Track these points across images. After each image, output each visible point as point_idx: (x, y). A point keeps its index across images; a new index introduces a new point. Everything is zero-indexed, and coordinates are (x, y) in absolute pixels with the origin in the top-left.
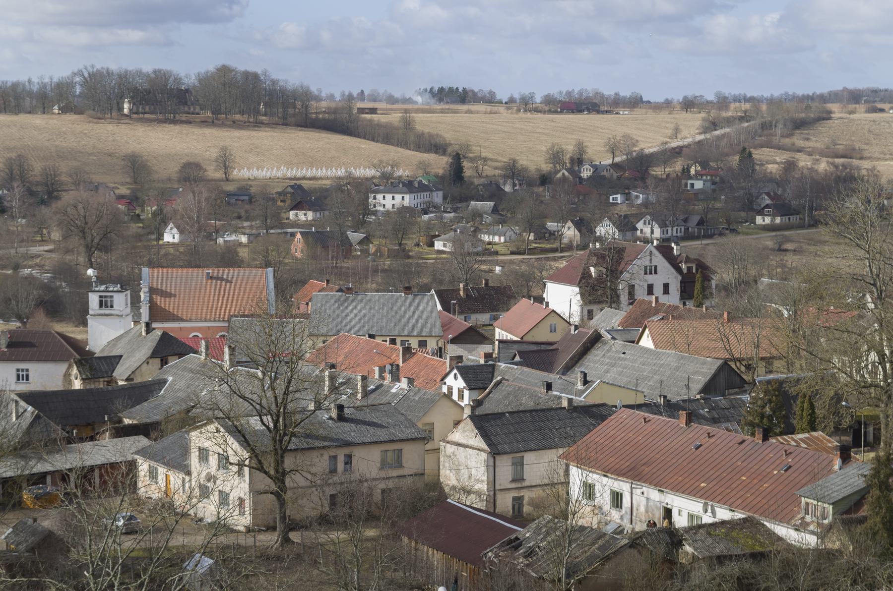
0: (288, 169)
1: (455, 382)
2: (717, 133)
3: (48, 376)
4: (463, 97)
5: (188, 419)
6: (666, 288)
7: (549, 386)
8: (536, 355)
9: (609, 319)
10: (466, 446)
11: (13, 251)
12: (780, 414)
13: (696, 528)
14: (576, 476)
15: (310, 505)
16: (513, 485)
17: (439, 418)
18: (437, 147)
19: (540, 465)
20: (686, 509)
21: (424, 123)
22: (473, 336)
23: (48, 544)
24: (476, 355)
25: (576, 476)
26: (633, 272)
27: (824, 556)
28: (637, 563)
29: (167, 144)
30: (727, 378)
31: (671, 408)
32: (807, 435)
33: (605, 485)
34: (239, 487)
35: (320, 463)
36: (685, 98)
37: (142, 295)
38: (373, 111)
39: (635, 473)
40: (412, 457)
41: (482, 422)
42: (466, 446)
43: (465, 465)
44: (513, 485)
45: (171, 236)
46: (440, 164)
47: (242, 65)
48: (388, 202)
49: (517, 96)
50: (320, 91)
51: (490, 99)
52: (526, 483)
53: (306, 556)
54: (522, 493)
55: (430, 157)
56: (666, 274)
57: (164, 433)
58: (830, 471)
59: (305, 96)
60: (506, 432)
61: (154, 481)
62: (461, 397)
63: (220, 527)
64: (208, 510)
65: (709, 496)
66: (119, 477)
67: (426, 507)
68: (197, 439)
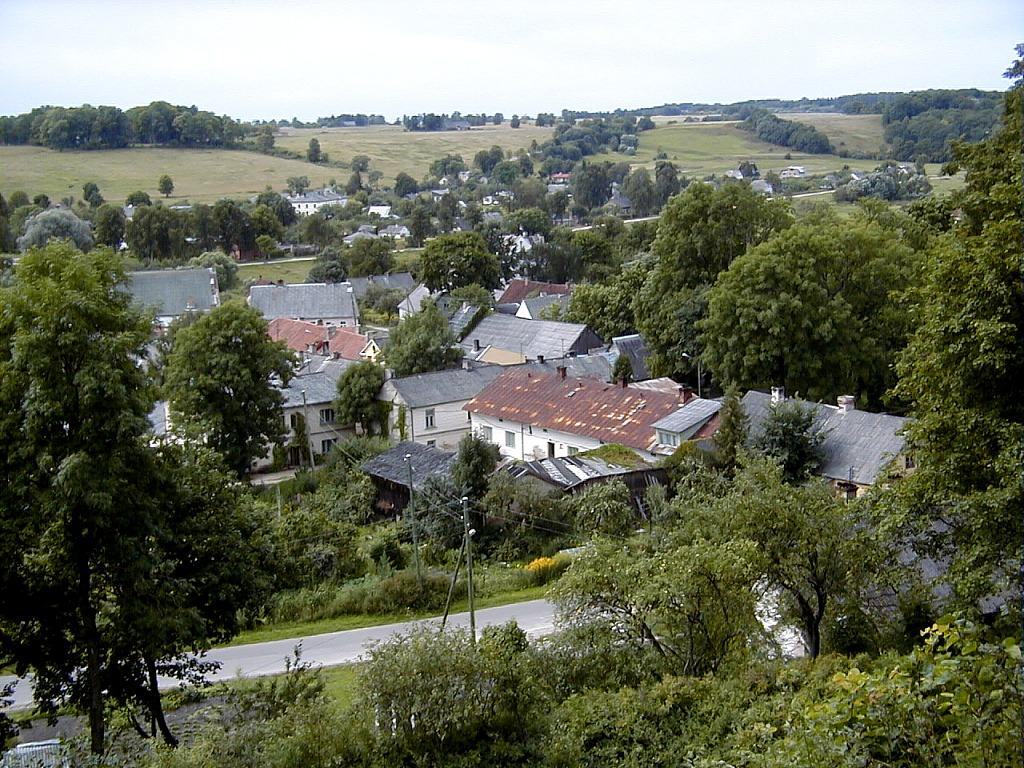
29: (124, 176)
51: (381, 120)
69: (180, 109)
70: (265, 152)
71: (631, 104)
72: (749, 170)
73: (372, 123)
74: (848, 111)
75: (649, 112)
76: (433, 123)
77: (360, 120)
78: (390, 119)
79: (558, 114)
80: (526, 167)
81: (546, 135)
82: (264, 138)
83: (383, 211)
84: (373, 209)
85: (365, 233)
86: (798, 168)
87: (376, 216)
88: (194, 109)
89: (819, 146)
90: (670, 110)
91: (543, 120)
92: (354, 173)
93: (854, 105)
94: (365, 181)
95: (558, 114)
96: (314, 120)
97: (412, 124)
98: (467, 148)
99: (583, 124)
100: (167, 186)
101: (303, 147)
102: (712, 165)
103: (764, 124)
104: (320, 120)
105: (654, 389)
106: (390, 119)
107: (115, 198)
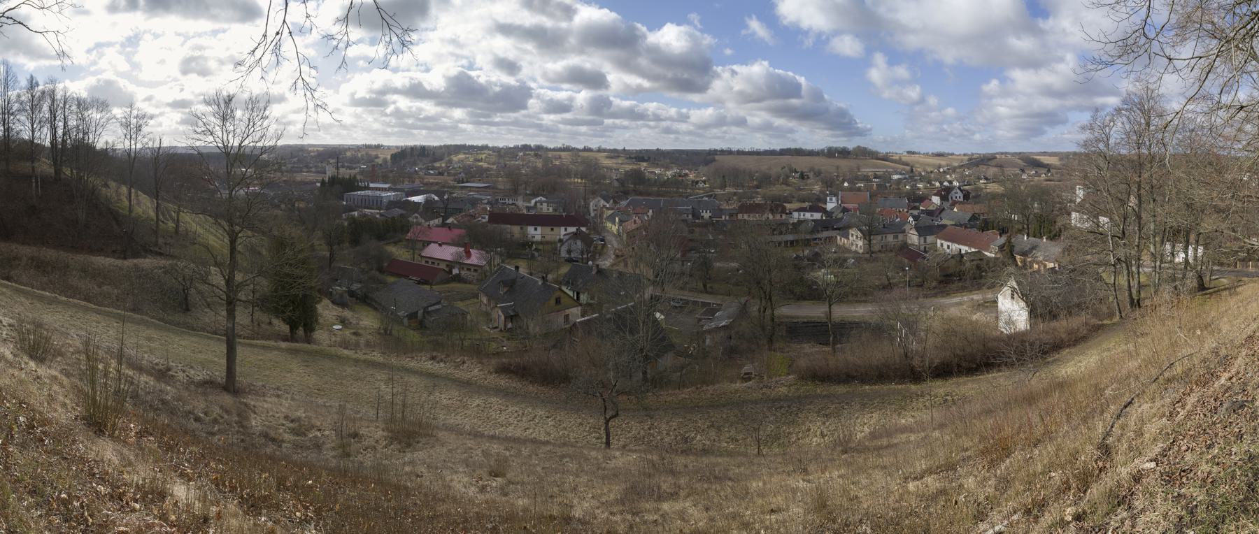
0: (333, 449)
1: (911, 219)
2: (346, 352)
3: (817, 216)
4: (914, 153)
5: (849, 227)
8: (930, 213)
9: (946, 205)
12: (986, 226)
13: (967, 253)
14: (939, 242)
15: (877, 248)
17: (907, 227)
18: (907, 164)
19: (930, 239)
20: (964, 249)
21: (904, 159)
22: (916, 208)
23: (817, 254)
24: (915, 212)
25: (939, 242)
26: (953, 194)
27: (996, 259)
28: (953, 262)
29: (844, 164)
30: (974, 218)
31: (961, 225)
33: (946, 244)
34: (860, 243)
35: (879, 237)
39: (953, 241)
40: (901, 237)
41: (917, 228)
43: (914, 238)
45: (846, 184)
46: (908, 168)
47: (862, 145)
48: (896, 177)
53: (875, 260)
56: (960, 194)
57: (844, 230)
59: (877, 153)
60: (923, 231)
61: (841, 241)
63: (856, 252)
64: (854, 248)
65: (970, 246)
66: (831, 240)
67: (904, 248)
68: (851, 232)
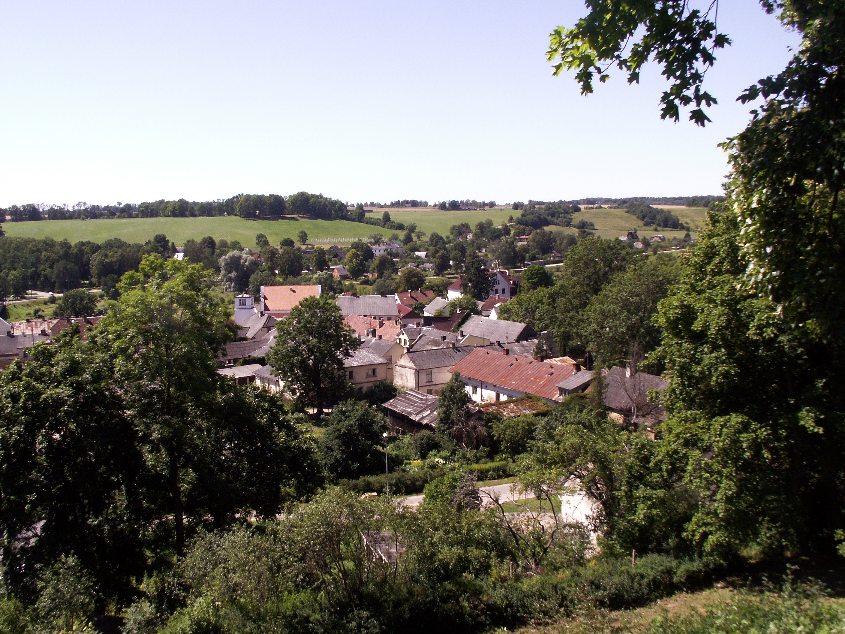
6: (504, 290)
7: (444, 338)
10: (405, 367)
11: (721, 561)
16: (428, 384)
29: (277, 232)
32: (561, 358)
36: (515, 203)
37: (316, 583)
38: (371, 211)
42: (405, 367)
44: (428, 384)
49: (437, 203)
50: (347, 203)
51: (425, 204)
52: (433, 383)
54: (432, 387)
55: (398, 232)
58: (571, 375)
62: (405, 343)
69: (313, 196)
70: (360, 221)
71: (568, 198)
72: (633, 236)
73: (345, 217)
74: (689, 205)
75: (579, 202)
76: (455, 206)
77: (414, 204)
78: (431, 203)
79: (526, 202)
80: (506, 231)
81: (518, 214)
82: (360, 214)
83: (422, 254)
84: (417, 253)
85: (411, 265)
86: (655, 235)
87: (418, 257)
88: (321, 196)
89: (670, 222)
90: (590, 201)
91: (516, 206)
92: (724, 195)
93: (693, 202)
94: (415, 238)
95: (526, 202)
96: (388, 203)
97: (443, 206)
98: (474, 219)
99: (539, 208)
100: (304, 237)
101: (380, 216)
102: (611, 230)
103: (644, 211)
104: (392, 203)
105: (559, 363)
106: (431, 203)
107: (275, 242)
